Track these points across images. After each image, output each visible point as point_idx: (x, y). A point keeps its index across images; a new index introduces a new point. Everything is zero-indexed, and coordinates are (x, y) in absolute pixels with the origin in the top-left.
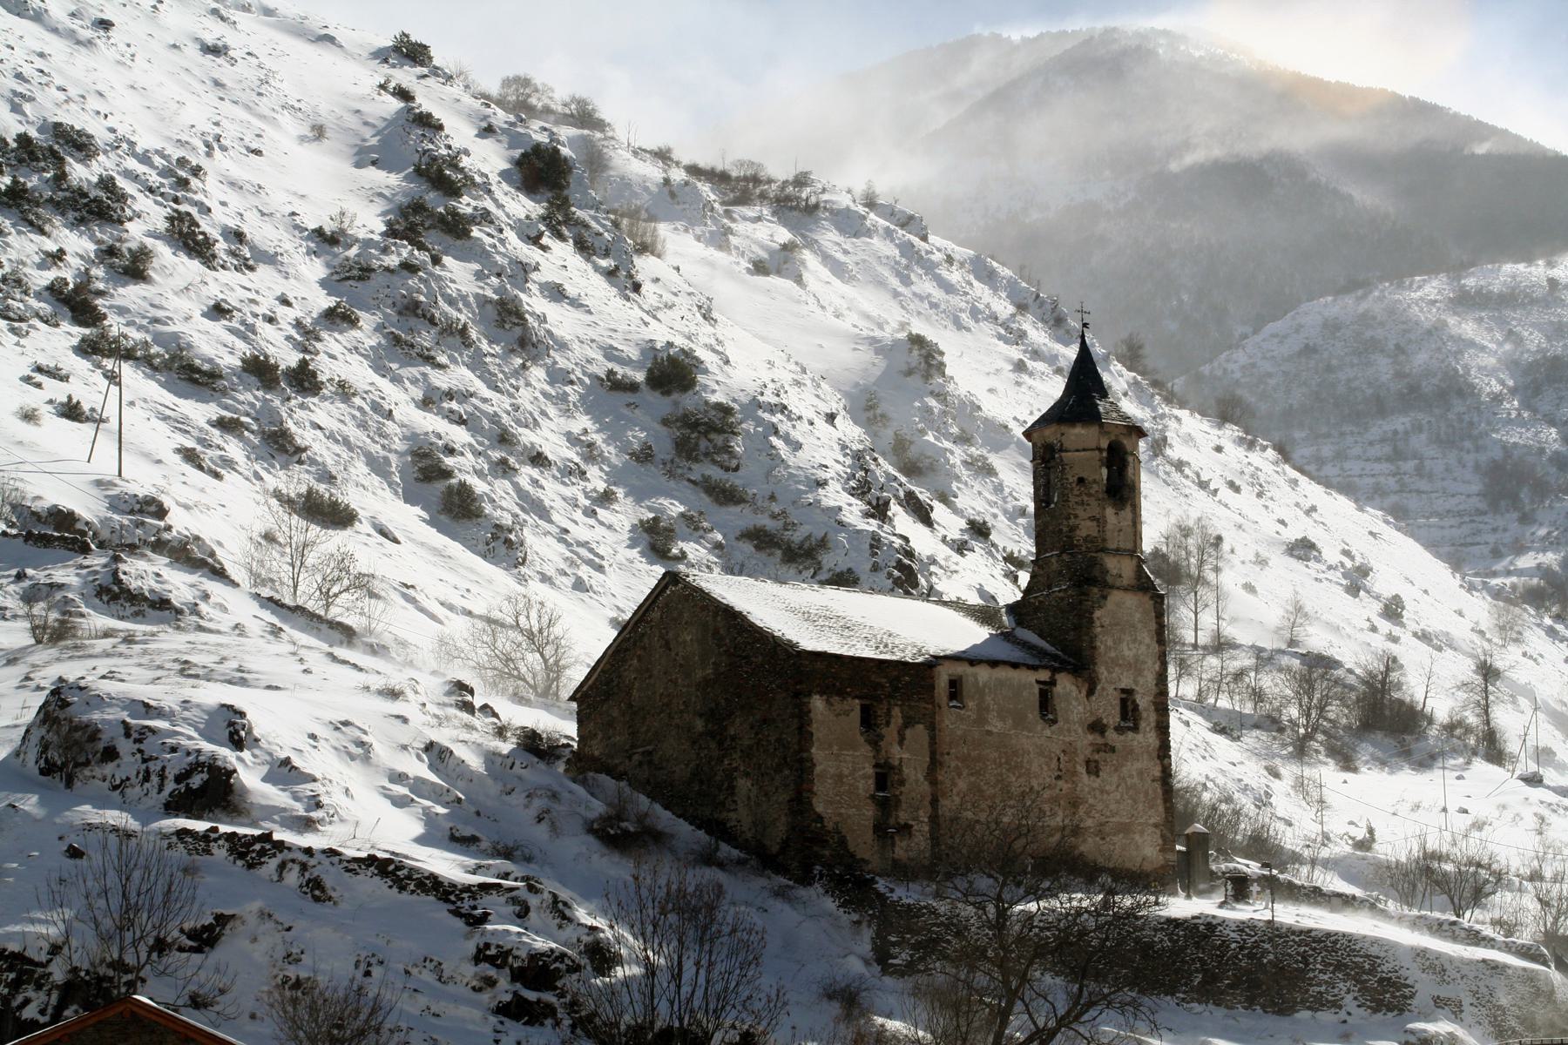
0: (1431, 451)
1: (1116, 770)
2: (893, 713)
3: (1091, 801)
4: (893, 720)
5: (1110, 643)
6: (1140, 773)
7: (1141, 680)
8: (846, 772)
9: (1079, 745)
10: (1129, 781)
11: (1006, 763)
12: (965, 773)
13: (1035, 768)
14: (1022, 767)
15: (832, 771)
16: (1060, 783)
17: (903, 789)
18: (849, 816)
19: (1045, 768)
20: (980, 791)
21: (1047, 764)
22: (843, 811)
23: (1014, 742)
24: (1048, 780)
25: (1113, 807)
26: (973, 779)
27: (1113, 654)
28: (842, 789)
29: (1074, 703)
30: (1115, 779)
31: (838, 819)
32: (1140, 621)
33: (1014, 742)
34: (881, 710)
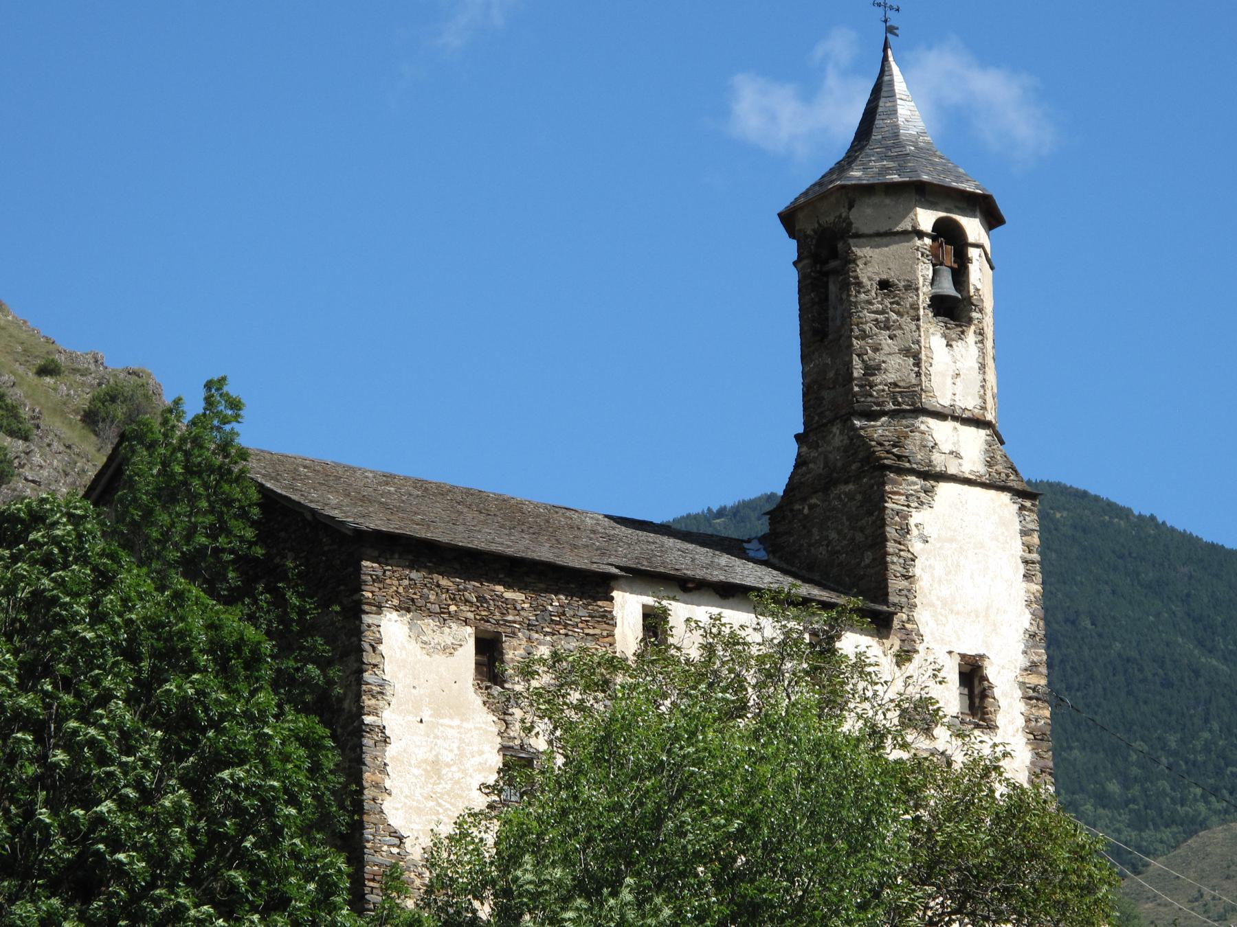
8: (447, 757)
28: (438, 789)
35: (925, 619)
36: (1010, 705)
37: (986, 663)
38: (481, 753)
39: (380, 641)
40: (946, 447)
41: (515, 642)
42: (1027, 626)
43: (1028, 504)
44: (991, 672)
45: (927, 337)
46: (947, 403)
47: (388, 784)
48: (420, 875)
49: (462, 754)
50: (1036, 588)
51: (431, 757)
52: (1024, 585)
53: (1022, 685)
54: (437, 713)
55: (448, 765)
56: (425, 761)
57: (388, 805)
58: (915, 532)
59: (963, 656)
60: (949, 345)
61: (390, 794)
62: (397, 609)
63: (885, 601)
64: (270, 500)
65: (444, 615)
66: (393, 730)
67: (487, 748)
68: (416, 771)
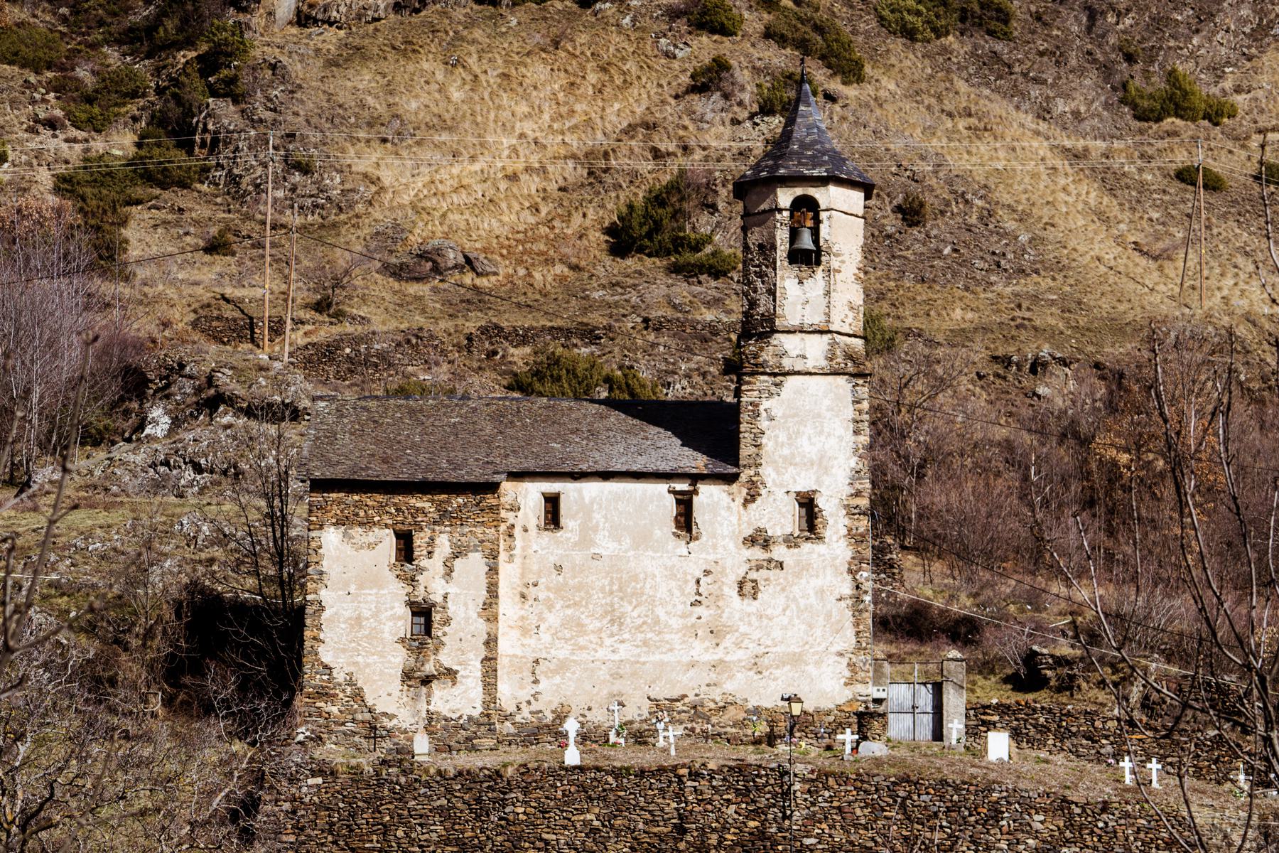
0: (936, 186)
1: (783, 590)
2: (437, 541)
3: (743, 629)
4: (437, 551)
5: (782, 437)
6: (821, 593)
7: (827, 480)
8: (366, 613)
9: (729, 563)
10: (802, 602)
11: (620, 589)
12: (558, 606)
13: (662, 593)
14: (642, 594)
15: (347, 614)
16: (698, 610)
17: (446, 629)
18: (368, 665)
19: (677, 593)
20: (580, 625)
21: (681, 589)
22: (360, 659)
23: (632, 564)
24: (681, 607)
25: (777, 634)
26: (569, 612)
27: (786, 451)
28: (359, 635)
29: (723, 512)
30: (781, 600)
31: (352, 669)
32: (829, 409)
33: (632, 564)
34: (420, 540)
35: (768, 473)
36: (836, 522)
37: (817, 496)
38: (392, 608)
39: (320, 547)
40: (794, 353)
41: (422, 534)
42: (853, 464)
43: (860, 382)
44: (821, 502)
45: (782, 278)
46: (797, 322)
47: (322, 636)
48: (344, 691)
49: (378, 611)
50: (864, 439)
51: (354, 615)
52: (853, 438)
53: (847, 507)
54: (361, 587)
55: (368, 619)
56: (350, 618)
57: (321, 649)
58: (764, 414)
59: (798, 494)
60: (801, 282)
61: (746, 502)
62: (334, 524)
63: (737, 465)
64: (302, 609)
65: (368, 523)
66: (329, 550)
67: (397, 604)
68: (343, 626)
